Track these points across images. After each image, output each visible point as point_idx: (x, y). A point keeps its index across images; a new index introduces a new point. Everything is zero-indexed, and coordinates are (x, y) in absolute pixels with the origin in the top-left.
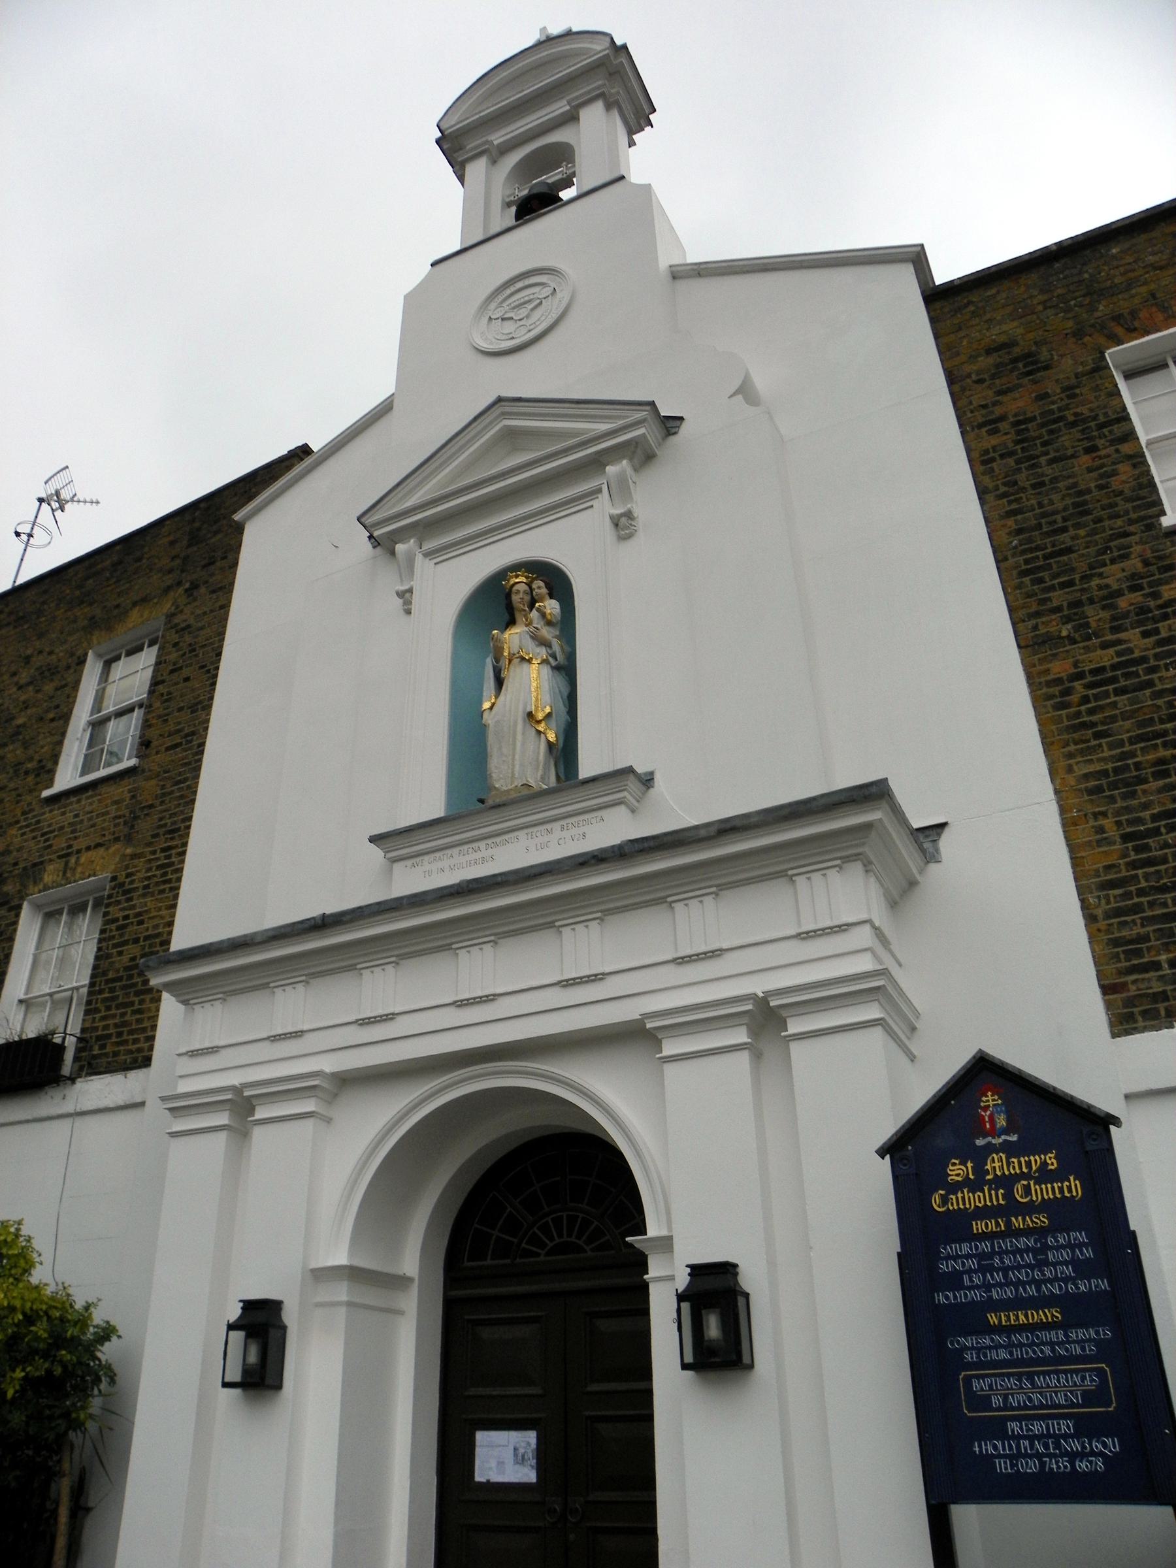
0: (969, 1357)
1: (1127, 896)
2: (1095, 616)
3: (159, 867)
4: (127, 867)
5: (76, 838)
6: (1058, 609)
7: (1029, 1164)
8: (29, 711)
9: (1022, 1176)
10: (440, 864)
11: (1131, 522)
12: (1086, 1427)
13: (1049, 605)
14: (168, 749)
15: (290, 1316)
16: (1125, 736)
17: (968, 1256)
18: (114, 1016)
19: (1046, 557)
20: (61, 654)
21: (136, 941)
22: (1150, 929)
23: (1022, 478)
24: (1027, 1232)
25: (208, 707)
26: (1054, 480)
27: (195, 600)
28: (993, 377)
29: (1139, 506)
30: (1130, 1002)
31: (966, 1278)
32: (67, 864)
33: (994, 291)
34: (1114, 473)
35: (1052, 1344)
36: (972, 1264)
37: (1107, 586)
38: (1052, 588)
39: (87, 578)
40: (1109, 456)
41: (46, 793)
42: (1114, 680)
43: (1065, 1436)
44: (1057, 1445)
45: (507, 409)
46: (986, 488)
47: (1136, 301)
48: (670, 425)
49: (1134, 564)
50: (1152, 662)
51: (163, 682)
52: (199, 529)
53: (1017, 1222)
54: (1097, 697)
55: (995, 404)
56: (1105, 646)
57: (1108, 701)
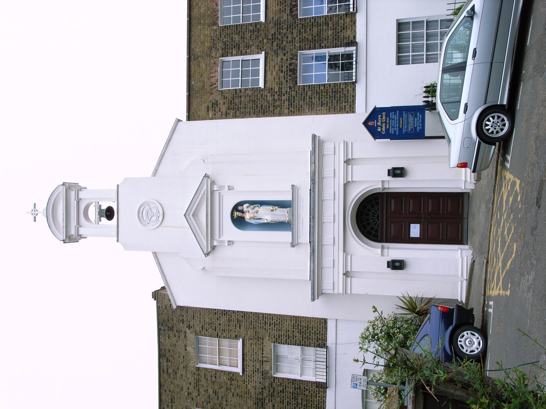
0: (406, 131)
1: (332, 108)
2: (278, 103)
6: (274, 110)
7: (380, 119)
9: (381, 120)
10: (301, 231)
11: (260, 93)
12: (416, 116)
13: (272, 111)
14: (240, 329)
15: (390, 259)
16: (303, 103)
17: (392, 130)
19: (262, 109)
21: (293, 331)
22: (338, 105)
23: (242, 111)
24: (389, 121)
29: (257, 91)
32: (265, 361)
33: (192, 108)
34: (248, 94)
35: (405, 119)
36: (393, 129)
37: (272, 100)
38: (269, 110)
40: (243, 94)
42: (291, 103)
43: (417, 119)
45: (188, 214)
48: (206, 176)
49: (269, 95)
50: (290, 95)
53: (388, 122)
54: (294, 106)
55: (222, 112)
56: (284, 103)
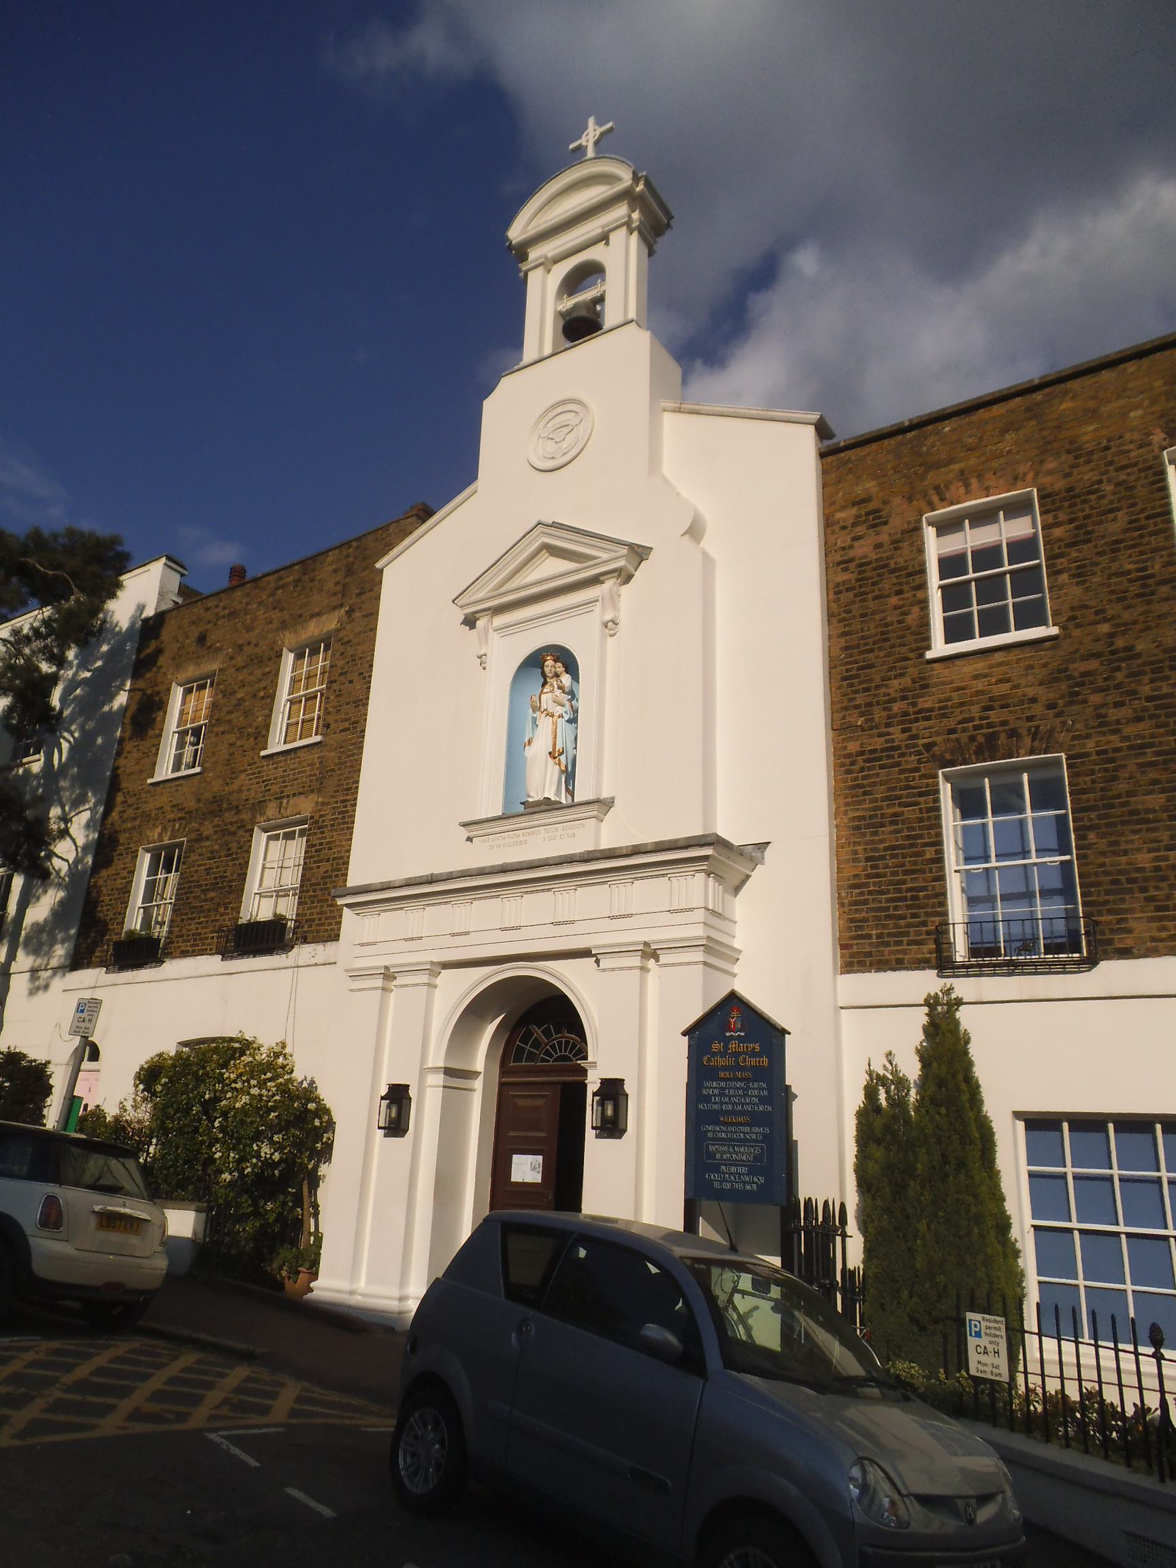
0: (710, 1135)
1: (862, 894)
2: (879, 714)
3: (339, 813)
4: (320, 810)
5: (285, 786)
7: (747, 1047)
8: (245, 689)
9: (744, 1053)
12: (752, 1171)
14: (341, 731)
17: (715, 1088)
18: (316, 907)
20: (264, 647)
21: (328, 860)
25: (365, 703)
26: (874, 613)
27: (353, 621)
28: (854, 525)
30: (852, 955)
31: (713, 1098)
32: (281, 803)
35: (744, 1133)
36: (716, 1091)
38: (857, 692)
39: (277, 589)
41: (263, 753)
44: (740, 1178)
46: (833, 612)
47: (951, 475)
49: (906, 681)
50: (904, 750)
51: (335, 681)
52: (353, 563)
53: (739, 1074)
56: (880, 735)
57: (875, 772)
